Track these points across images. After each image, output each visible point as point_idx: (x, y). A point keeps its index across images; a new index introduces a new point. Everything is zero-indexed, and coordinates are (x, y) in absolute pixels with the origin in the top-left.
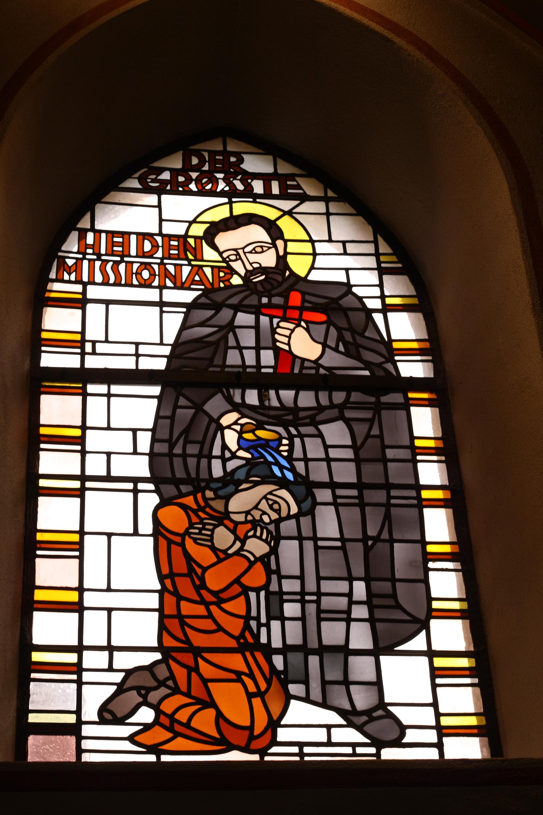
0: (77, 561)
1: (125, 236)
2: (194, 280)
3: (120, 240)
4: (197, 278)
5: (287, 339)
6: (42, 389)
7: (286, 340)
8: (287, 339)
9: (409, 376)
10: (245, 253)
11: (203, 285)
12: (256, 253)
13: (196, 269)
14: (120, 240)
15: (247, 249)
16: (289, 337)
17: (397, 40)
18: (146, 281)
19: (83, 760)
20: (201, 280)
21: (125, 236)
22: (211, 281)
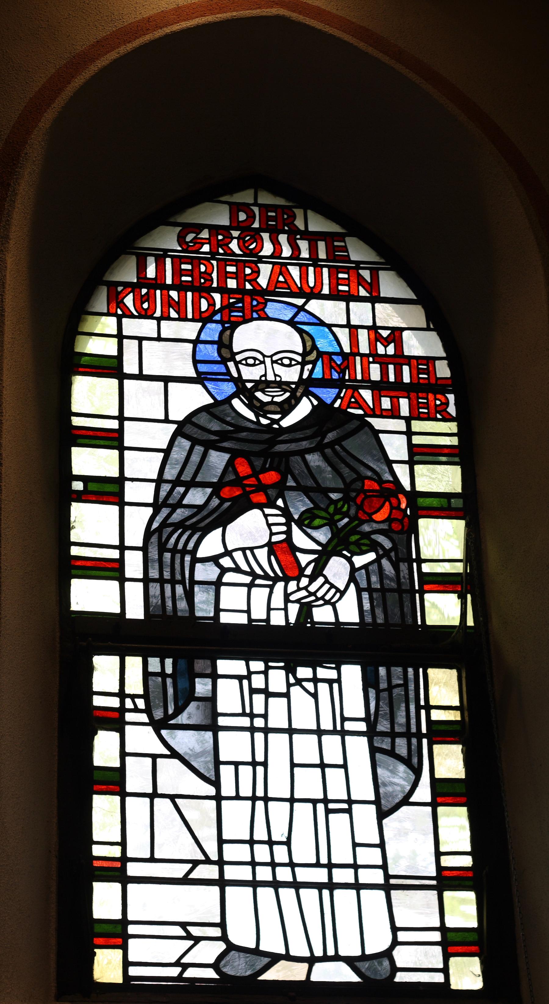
0: (240, 711)
1: (194, 261)
2: (278, 282)
3: (189, 267)
4: (281, 279)
5: (270, 522)
6: (74, 572)
7: (271, 520)
8: (270, 522)
9: (93, 687)
10: (273, 362)
11: (289, 288)
12: (283, 365)
13: (277, 268)
14: (189, 267)
15: (275, 358)
16: (269, 525)
17: (107, 617)
18: (210, 303)
19: (73, 503)
20: (286, 282)
21: (194, 261)
22: (299, 286)
